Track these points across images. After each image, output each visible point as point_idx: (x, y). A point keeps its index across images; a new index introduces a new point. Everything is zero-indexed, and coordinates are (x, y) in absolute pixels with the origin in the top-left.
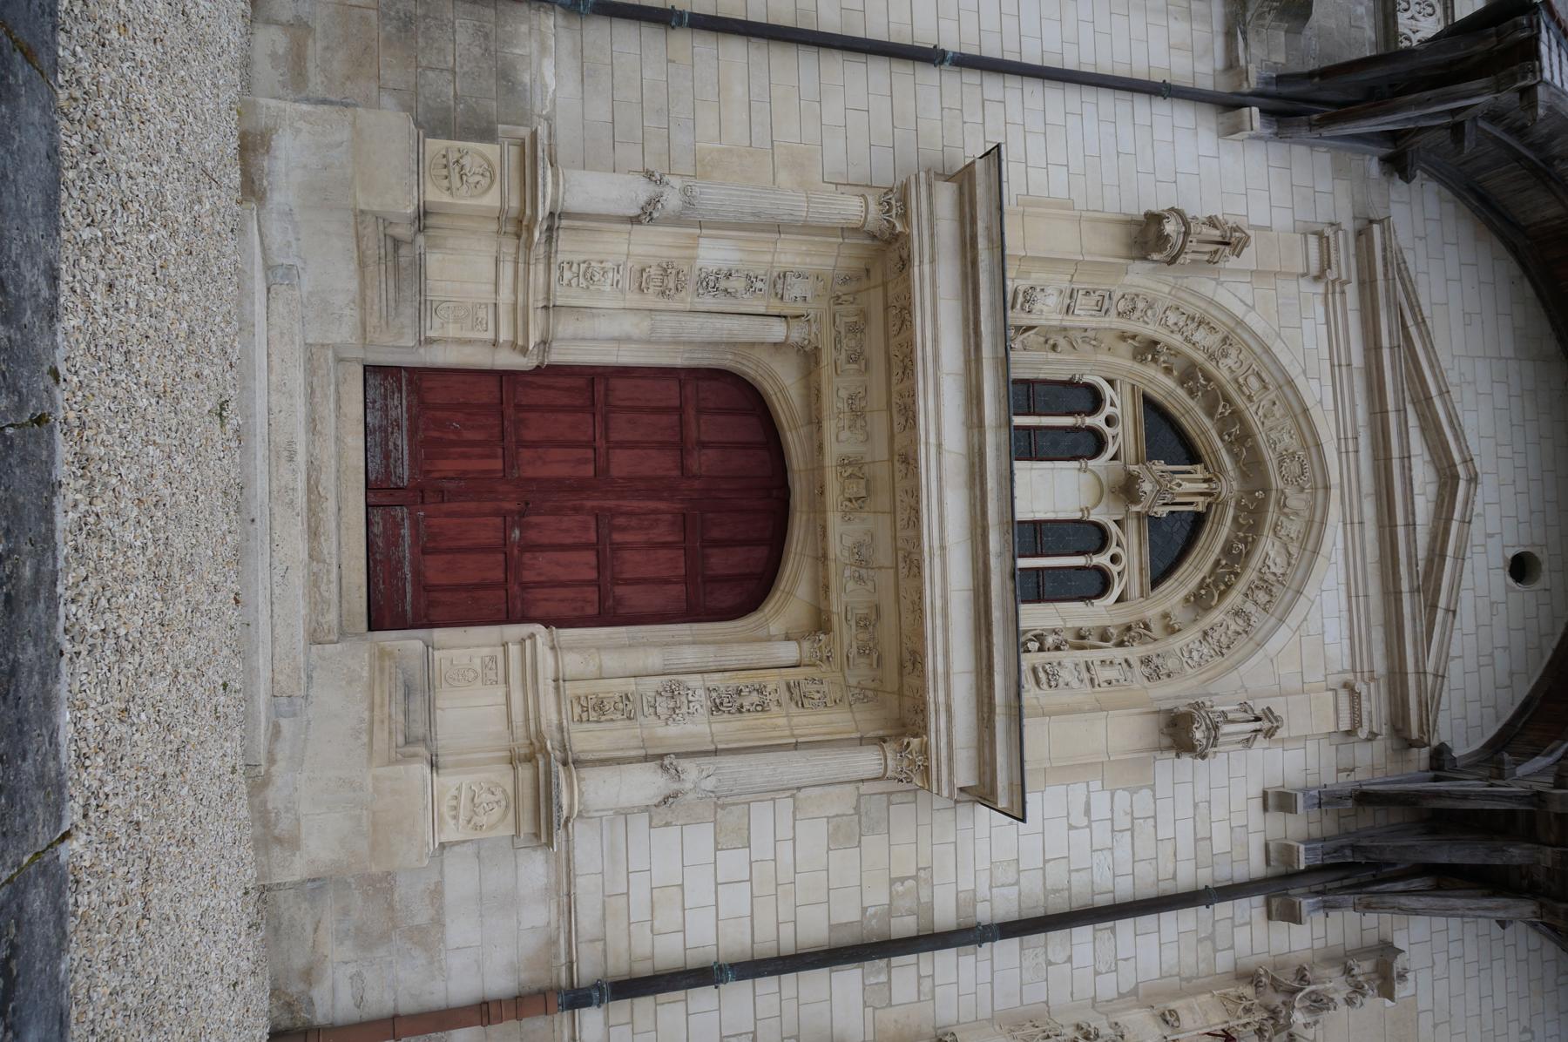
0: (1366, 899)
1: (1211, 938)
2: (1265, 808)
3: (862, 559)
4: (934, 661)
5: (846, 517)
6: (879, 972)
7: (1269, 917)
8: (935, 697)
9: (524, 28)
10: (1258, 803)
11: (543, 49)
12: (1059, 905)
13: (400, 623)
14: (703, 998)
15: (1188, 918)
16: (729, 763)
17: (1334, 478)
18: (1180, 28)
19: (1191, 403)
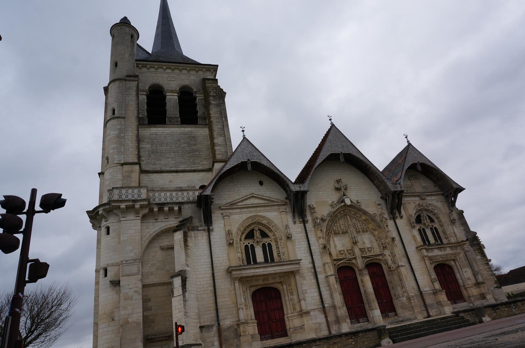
0: (305, 212)
1: (311, 231)
2: (296, 224)
3: (274, 278)
4: (286, 270)
5: (269, 281)
6: (318, 273)
7: (308, 223)
8: (290, 270)
9: (223, 327)
10: (295, 225)
11: (225, 324)
12: (309, 251)
13: (287, 333)
14: (322, 293)
15: (309, 234)
16: (299, 293)
17: (255, 214)
18: (200, 238)
19: (245, 232)
